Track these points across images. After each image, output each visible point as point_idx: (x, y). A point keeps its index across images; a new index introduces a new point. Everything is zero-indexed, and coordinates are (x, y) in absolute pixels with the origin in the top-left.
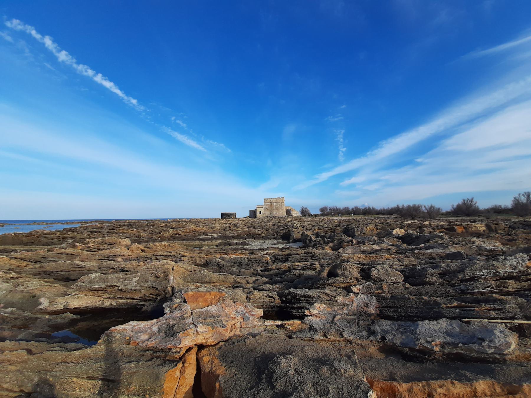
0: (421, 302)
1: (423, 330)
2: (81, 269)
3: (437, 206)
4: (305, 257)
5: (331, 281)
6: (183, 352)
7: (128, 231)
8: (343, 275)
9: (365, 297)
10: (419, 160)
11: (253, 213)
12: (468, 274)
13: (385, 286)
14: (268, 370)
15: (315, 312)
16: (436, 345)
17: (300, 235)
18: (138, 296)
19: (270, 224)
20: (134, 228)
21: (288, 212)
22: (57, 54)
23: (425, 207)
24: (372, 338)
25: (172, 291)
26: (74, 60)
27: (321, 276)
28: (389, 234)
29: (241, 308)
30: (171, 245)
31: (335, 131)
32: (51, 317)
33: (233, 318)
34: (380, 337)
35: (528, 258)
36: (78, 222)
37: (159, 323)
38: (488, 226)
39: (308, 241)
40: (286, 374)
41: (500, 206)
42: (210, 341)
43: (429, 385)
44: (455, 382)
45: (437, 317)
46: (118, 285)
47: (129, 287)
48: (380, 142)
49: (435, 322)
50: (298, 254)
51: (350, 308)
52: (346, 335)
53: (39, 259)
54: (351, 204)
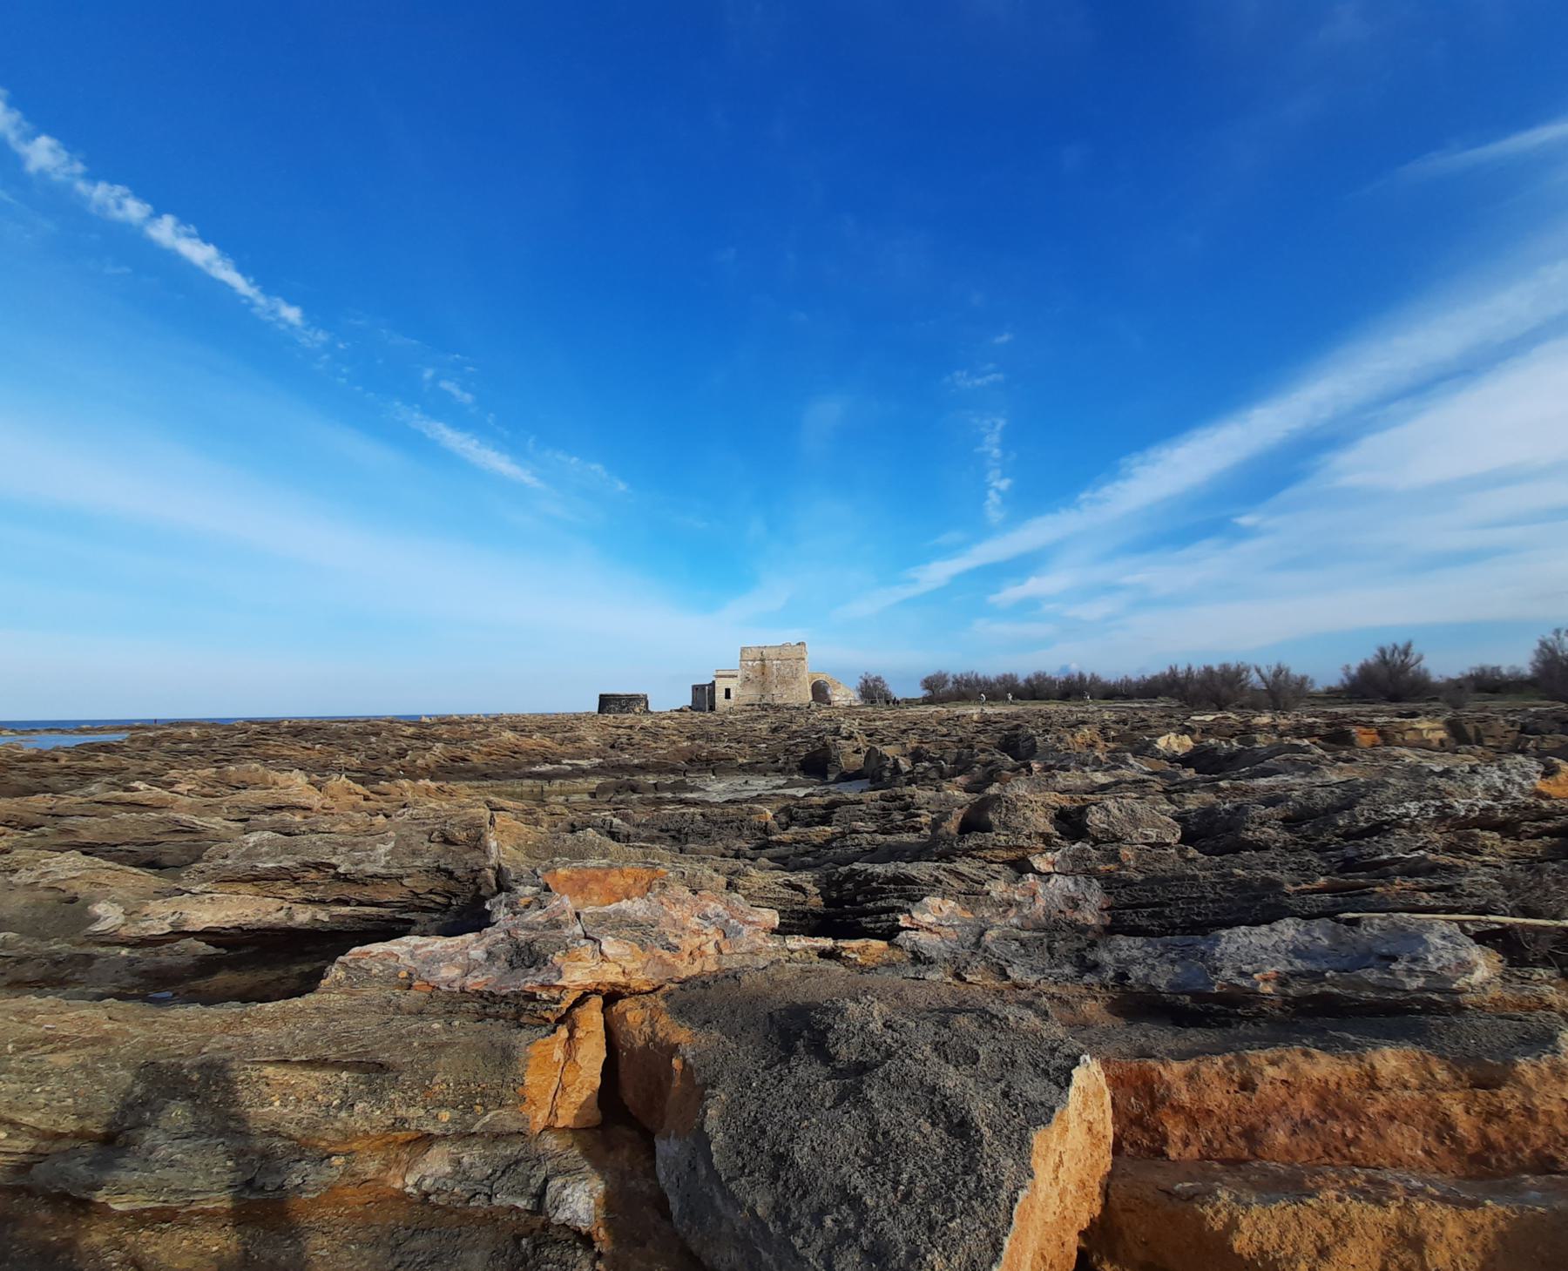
0: (1229, 883)
1: (1232, 948)
2: (191, 837)
3: (1297, 670)
4: (884, 809)
5: (971, 842)
6: (569, 999)
7: (296, 751)
8: (1006, 826)
9: (1069, 883)
10: (1246, 521)
11: (704, 696)
12: (1363, 814)
13: (1126, 852)
14: (811, 1029)
15: (928, 919)
16: (1266, 980)
17: (860, 758)
18: (392, 894)
19: (763, 727)
20: (315, 742)
21: (820, 691)
22: (24, 149)
23: (1258, 671)
24: (1088, 978)
25: (497, 880)
26: (79, 168)
27: (941, 831)
28: (1144, 750)
29: (714, 907)
30: (446, 788)
31: (976, 421)
32: (137, 954)
33: (697, 933)
34: (1111, 974)
35: (1541, 769)
36: (119, 726)
37: (487, 940)
38: (1455, 728)
39: (887, 774)
40: (862, 1029)
41: (1497, 670)
42: (639, 980)
43: (1242, 1061)
44: (1314, 1051)
45: (1269, 916)
46: (334, 861)
47: (370, 869)
48: (1123, 460)
49: (1264, 928)
50: (860, 802)
51: (1026, 911)
52: (1016, 973)
53: (36, 819)
54: (1023, 667)
